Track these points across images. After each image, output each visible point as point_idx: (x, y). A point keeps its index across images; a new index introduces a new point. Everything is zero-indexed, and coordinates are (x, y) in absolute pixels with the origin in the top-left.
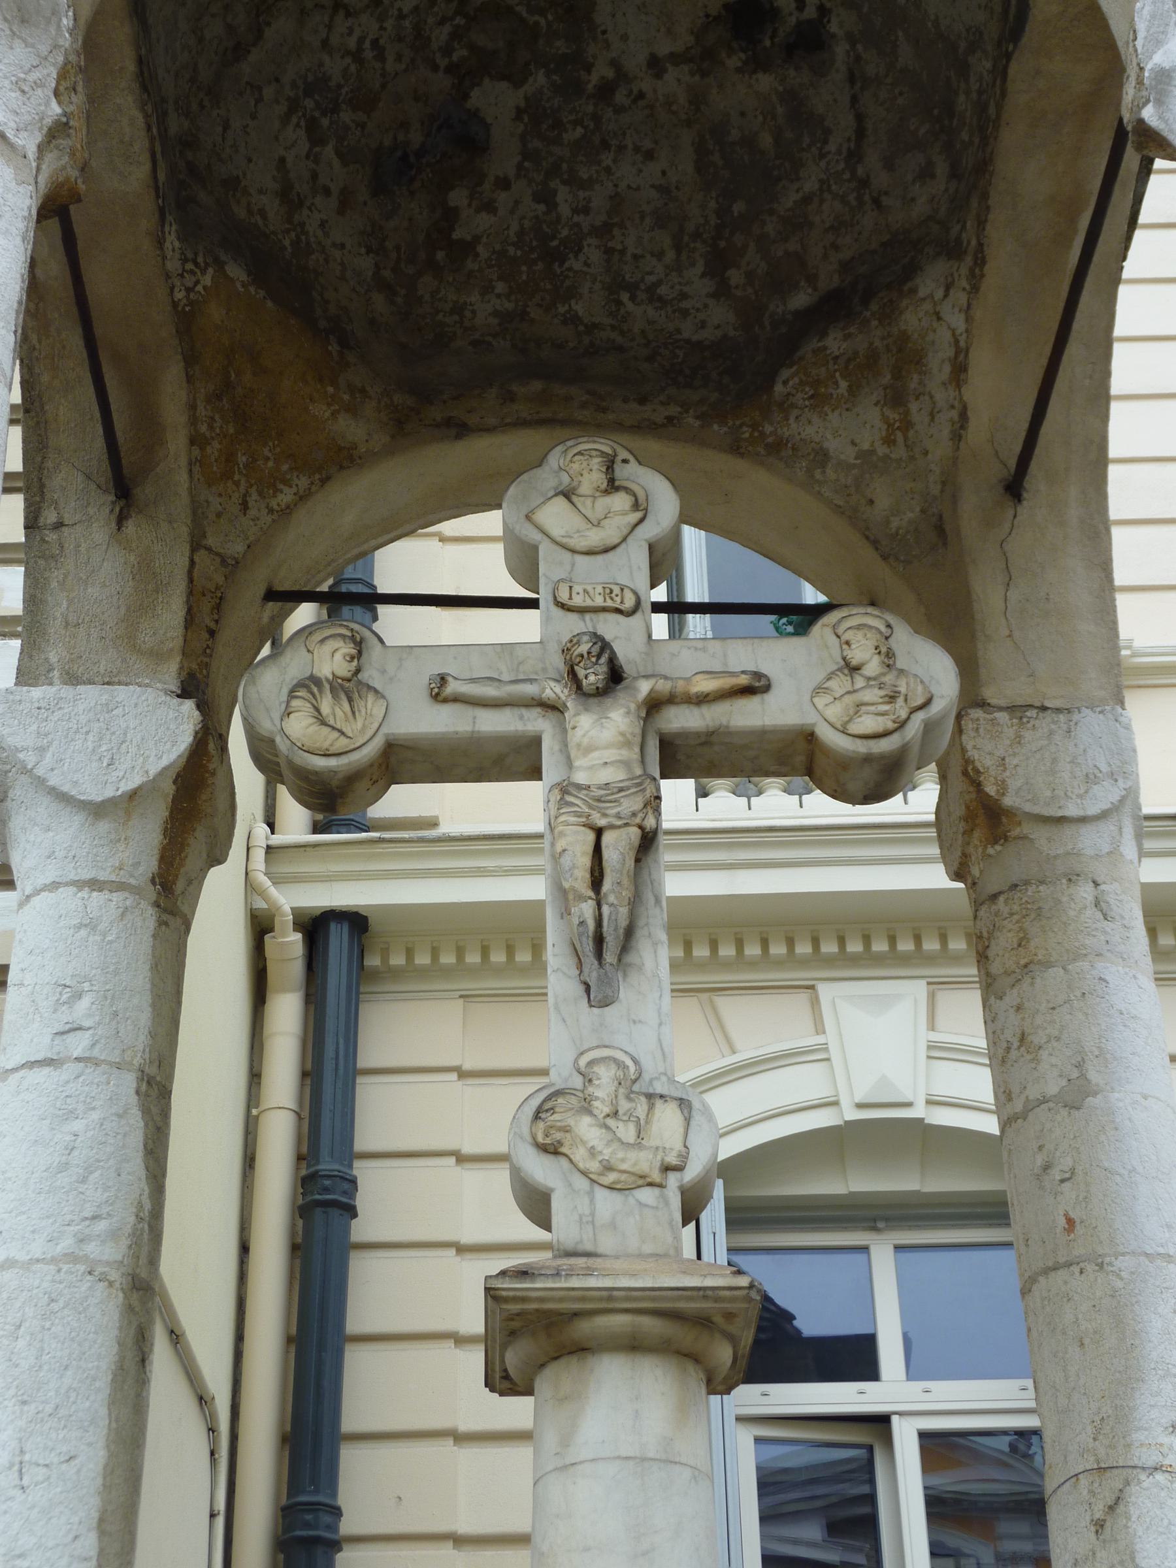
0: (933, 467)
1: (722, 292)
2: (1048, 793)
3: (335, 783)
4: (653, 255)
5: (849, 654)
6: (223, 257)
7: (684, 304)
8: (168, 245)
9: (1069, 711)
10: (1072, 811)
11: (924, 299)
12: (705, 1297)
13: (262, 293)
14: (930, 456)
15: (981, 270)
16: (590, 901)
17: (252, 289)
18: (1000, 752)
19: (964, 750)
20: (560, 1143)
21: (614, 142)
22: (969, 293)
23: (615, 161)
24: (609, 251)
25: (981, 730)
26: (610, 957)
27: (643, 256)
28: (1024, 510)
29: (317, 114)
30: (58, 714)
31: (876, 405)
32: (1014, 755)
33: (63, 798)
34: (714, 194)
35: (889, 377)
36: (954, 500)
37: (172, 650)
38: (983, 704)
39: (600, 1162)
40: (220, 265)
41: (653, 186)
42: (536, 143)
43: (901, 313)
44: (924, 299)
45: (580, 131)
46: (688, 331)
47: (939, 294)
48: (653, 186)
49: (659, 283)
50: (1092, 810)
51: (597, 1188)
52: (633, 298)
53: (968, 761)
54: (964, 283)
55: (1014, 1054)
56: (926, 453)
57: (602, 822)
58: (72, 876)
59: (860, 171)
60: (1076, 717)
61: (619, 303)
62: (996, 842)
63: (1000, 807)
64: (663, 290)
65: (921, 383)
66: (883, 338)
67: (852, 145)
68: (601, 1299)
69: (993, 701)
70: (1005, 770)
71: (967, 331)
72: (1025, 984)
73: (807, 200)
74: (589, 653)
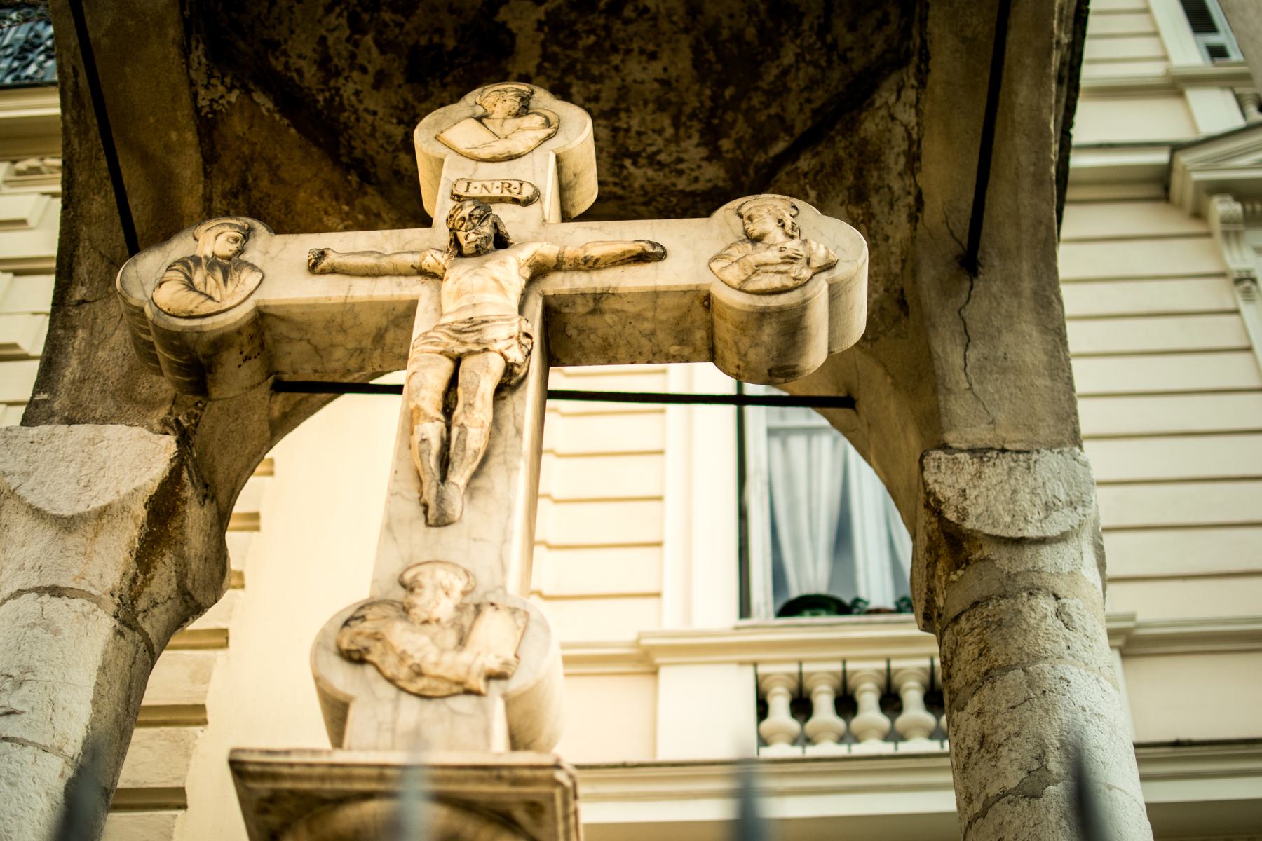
0: (894, 249)
1: (715, 155)
2: (1008, 519)
3: (200, 350)
4: (654, 131)
5: (750, 227)
6: (252, 86)
7: (681, 166)
8: (194, 57)
9: (1028, 452)
10: (1031, 532)
11: (880, 108)
12: (500, 778)
13: (286, 121)
14: (891, 241)
15: (927, 65)
16: (437, 423)
17: (277, 117)
18: (963, 485)
19: (925, 484)
20: (367, 650)
21: (622, 47)
22: (917, 88)
23: (623, 61)
24: (615, 130)
25: (943, 467)
26: (459, 477)
27: (645, 133)
28: (979, 284)
29: (359, 9)
30: (47, 447)
31: (842, 204)
32: (975, 487)
33: (38, 513)
34: (709, 84)
35: (851, 178)
36: (914, 273)
37: (164, 400)
38: (945, 447)
39: (410, 667)
40: (247, 92)
41: (656, 80)
42: (556, 49)
43: (861, 124)
44: (880, 108)
45: (592, 39)
46: (682, 183)
47: (893, 98)
48: (656, 80)
49: (659, 152)
50: (1053, 531)
51: (404, 696)
52: (635, 164)
53: (929, 494)
54: (913, 82)
55: (974, 756)
56: (887, 238)
57: (460, 349)
58: (35, 584)
59: (829, 39)
60: (1035, 456)
61: (622, 167)
62: (958, 567)
63: (961, 532)
64: (662, 157)
65: (880, 178)
66: (845, 148)
67: (822, 20)
68: (369, 779)
69: (955, 445)
70: (966, 499)
71: (918, 124)
72: (986, 691)
73: (785, 72)
74: (471, 216)
